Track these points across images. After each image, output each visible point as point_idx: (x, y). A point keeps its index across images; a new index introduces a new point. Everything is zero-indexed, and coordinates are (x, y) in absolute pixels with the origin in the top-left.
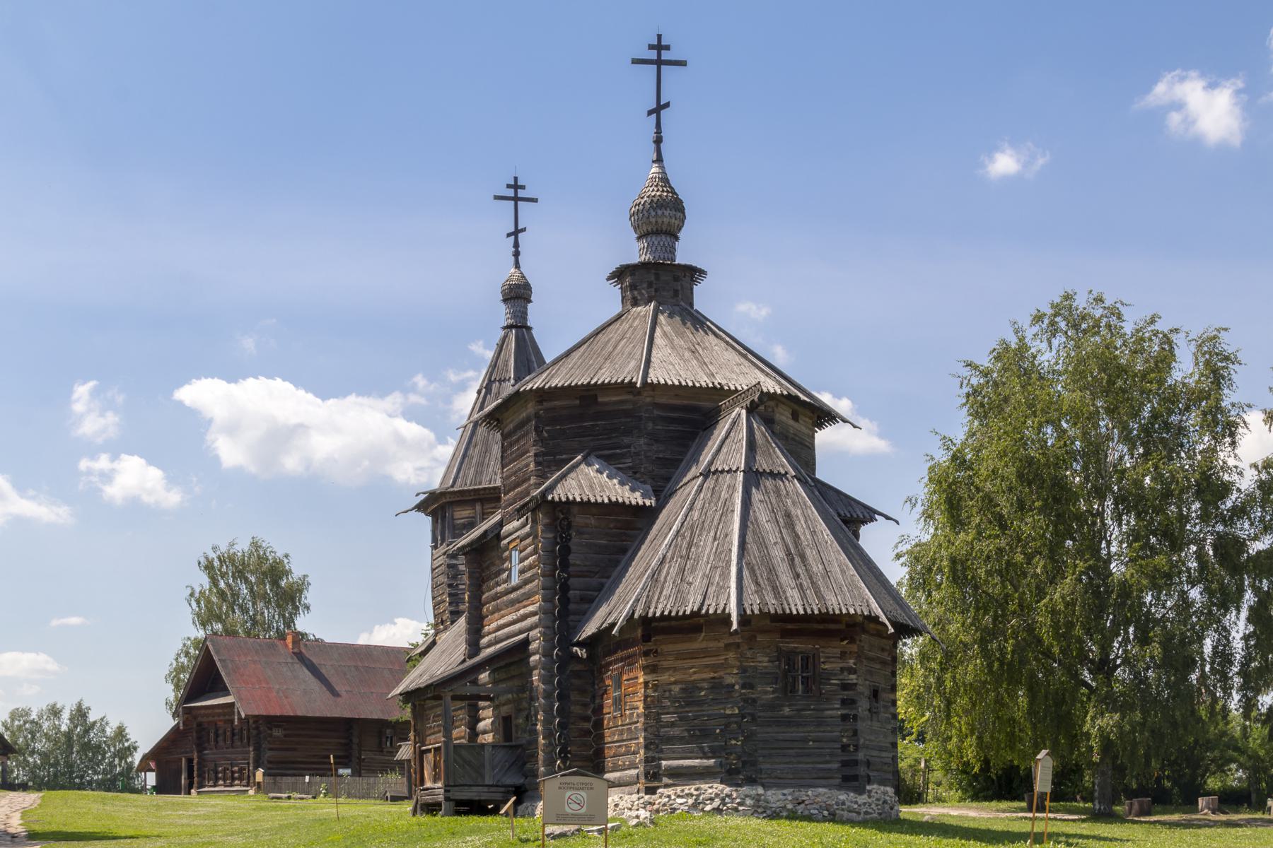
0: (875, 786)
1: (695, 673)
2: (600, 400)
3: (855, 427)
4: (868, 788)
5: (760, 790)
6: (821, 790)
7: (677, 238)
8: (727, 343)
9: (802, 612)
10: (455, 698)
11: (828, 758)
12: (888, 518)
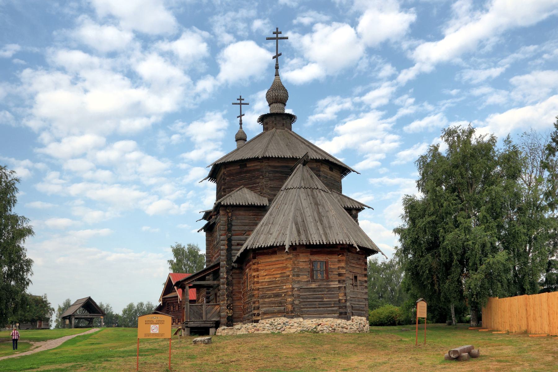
0: (356, 317)
2: (248, 166)
4: (352, 317)
5: (301, 320)
6: (329, 319)
7: (285, 105)
8: (300, 140)
10: (190, 287)
12: (369, 208)
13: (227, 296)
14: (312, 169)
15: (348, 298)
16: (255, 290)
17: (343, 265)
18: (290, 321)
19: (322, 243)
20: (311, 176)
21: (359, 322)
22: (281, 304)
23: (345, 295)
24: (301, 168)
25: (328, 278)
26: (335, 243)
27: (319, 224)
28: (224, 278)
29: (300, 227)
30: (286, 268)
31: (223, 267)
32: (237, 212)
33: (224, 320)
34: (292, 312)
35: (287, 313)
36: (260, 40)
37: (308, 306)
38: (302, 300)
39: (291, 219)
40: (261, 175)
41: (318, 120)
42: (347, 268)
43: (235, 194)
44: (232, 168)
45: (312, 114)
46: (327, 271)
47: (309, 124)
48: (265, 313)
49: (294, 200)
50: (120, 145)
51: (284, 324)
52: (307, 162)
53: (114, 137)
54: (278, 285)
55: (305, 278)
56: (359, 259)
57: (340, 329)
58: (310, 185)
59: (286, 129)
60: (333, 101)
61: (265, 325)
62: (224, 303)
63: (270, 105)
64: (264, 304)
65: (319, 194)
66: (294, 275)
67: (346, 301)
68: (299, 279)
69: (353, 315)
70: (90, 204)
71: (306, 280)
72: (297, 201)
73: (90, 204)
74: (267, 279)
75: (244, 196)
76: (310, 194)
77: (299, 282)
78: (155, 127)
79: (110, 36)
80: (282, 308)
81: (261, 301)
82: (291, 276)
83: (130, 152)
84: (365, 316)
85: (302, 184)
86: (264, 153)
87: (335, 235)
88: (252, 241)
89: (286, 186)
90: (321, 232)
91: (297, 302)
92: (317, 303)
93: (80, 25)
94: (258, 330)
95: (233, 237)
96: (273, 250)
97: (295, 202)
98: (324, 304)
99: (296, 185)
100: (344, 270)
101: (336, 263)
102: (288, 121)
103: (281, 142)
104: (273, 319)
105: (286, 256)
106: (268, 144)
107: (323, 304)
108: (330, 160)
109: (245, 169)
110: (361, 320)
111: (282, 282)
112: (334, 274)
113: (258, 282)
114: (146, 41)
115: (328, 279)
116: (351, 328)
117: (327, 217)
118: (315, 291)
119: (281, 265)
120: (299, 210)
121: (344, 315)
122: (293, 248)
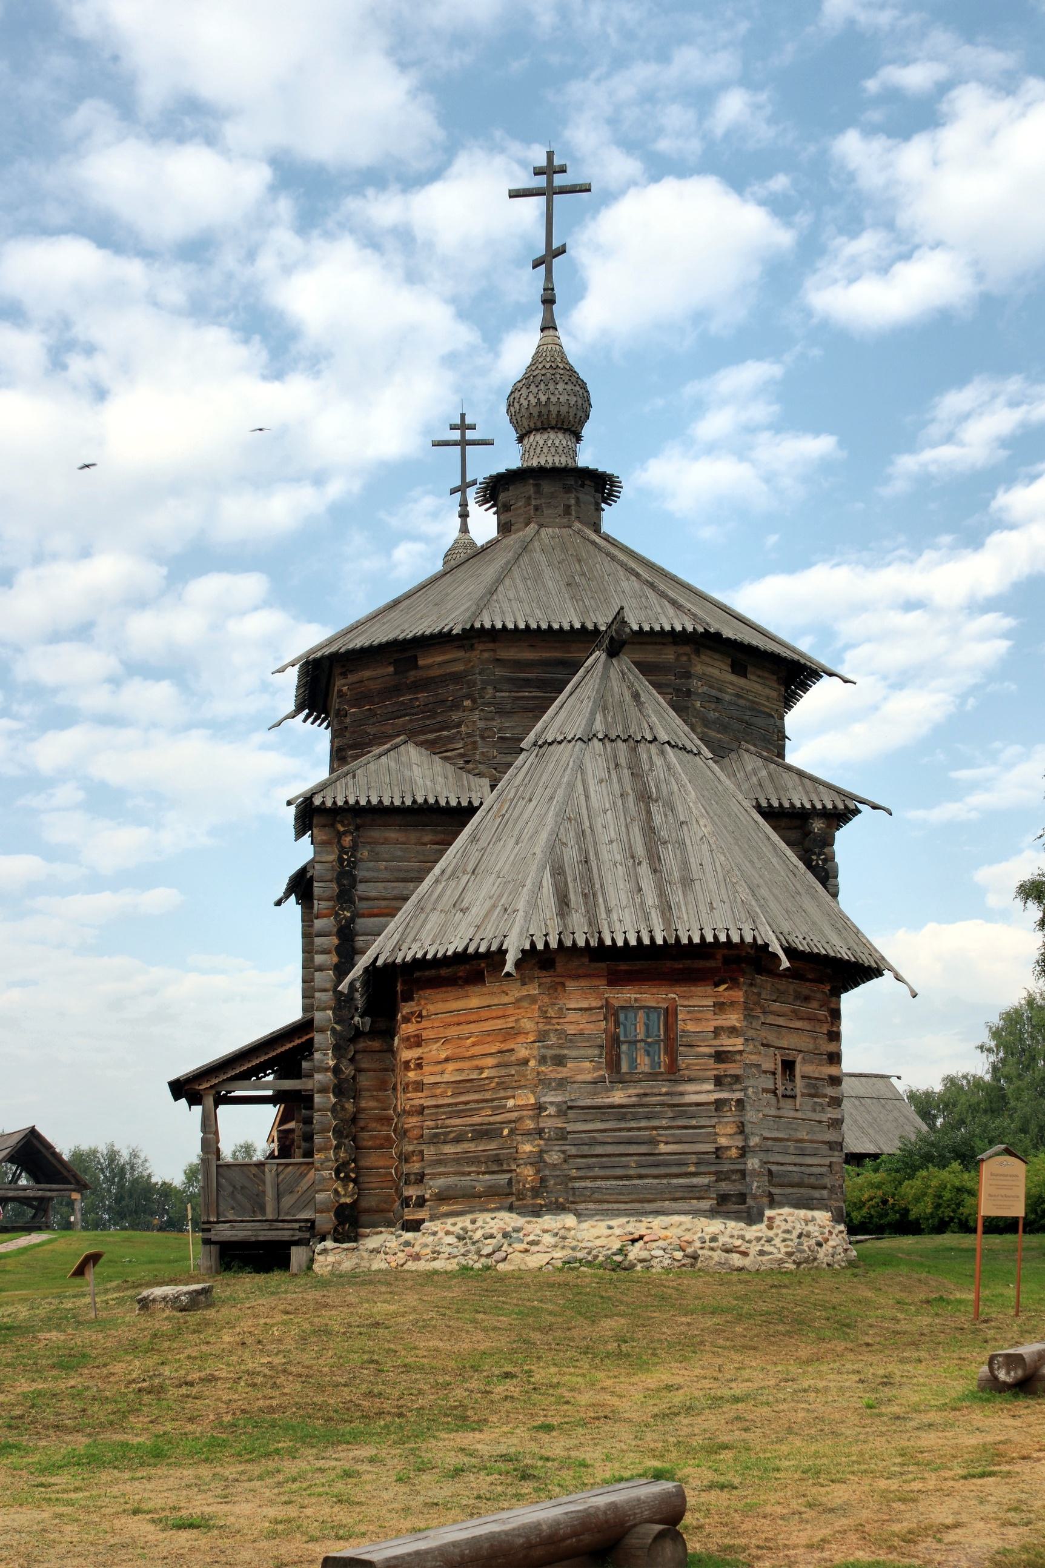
0: (786, 1211)
1: (474, 1045)
2: (421, 663)
3: (846, 681)
4: (768, 1213)
5: (570, 1220)
6: (676, 1218)
7: (578, 438)
8: (623, 565)
9: (608, 942)
11: (692, 1169)
12: (875, 807)
13: (338, 1133)
14: (645, 668)
15: (754, 1141)
16: (409, 1113)
17: (733, 1019)
18: (529, 1228)
19: (646, 941)
20: (636, 696)
21: (799, 1228)
22: (497, 1163)
23: (741, 1129)
24: (599, 667)
25: (673, 1067)
26: (696, 940)
27: (644, 870)
28: (327, 1070)
29: (572, 880)
30: (512, 1033)
31: (322, 1030)
32: (376, 834)
33: (326, 1221)
34: (536, 1192)
35: (521, 1196)
36: (735, 167)
37: (597, 1172)
38: (573, 1151)
39: (539, 855)
40: (469, 696)
41: (933, 469)
42: (751, 1033)
43: (372, 766)
44: (367, 674)
45: (911, 446)
46: (671, 1043)
47: (899, 486)
48: (442, 1197)
49: (559, 785)
50: (209, 587)
51: (506, 1235)
52: (623, 644)
53: (190, 561)
54: (488, 1095)
55: (584, 1068)
56: (807, 999)
57: (718, 1255)
58: (626, 729)
59: (577, 525)
60: (994, 396)
61: (441, 1242)
62: (327, 1159)
63: (520, 440)
64: (439, 1162)
65: (658, 761)
66: (543, 1060)
67: (744, 1151)
68: (563, 1072)
69: (773, 1203)
70: (105, 801)
71: (589, 1077)
72: (571, 786)
73: (105, 801)
74: (450, 1073)
75: (410, 773)
76: (623, 761)
77: (562, 1084)
78: (341, 515)
79: (202, 185)
80: (503, 1178)
81: (429, 1151)
82: (532, 1063)
83: (243, 613)
84: (827, 1208)
85: (599, 726)
86: (478, 613)
87: (704, 909)
88: (396, 937)
89: (538, 736)
90: (651, 899)
91: (553, 1157)
92: (632, 1161)
93: (75, 147)
94: (417, 1257)
95: (359, 921)
96: (471, 968)
97: (560, 793)
98: (657, 1165)
99: (576, 729)
100: (741, 1040)
101: (705, 1015)
102: (587, 496)
103: (547, 573)
104: (469, 1217)
105: (516, 991)
106: (499, 581)
107: (654, 1163)
108: (728, 633)
109: (412, 675)
110: (807, 1222)
111: (502, 1086)
112: (699, 1056)
113: (419, 1086)
114: (312, 192)
115: (673, 1072)
116: (762, 1253)
117: (681, 844)
118: (623, 1118)
119: (499, 1024)
120: (576, 824)
121: (736, 1203)
122: (539, 960)
